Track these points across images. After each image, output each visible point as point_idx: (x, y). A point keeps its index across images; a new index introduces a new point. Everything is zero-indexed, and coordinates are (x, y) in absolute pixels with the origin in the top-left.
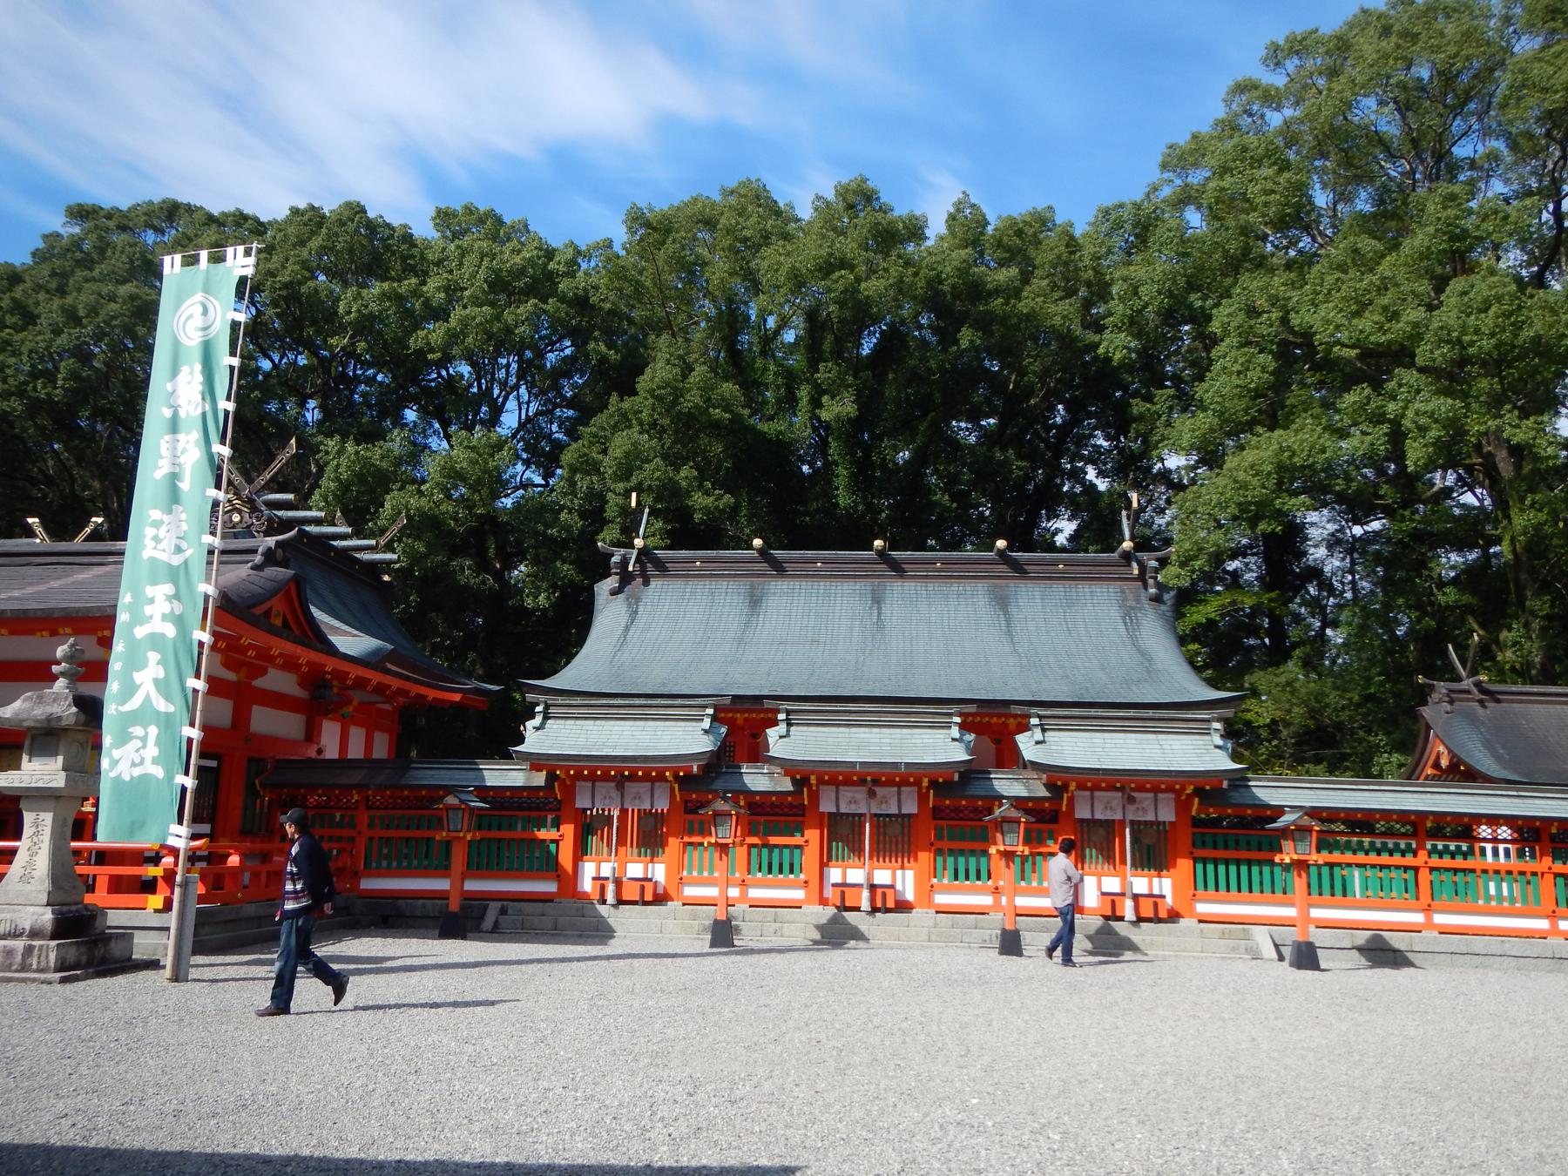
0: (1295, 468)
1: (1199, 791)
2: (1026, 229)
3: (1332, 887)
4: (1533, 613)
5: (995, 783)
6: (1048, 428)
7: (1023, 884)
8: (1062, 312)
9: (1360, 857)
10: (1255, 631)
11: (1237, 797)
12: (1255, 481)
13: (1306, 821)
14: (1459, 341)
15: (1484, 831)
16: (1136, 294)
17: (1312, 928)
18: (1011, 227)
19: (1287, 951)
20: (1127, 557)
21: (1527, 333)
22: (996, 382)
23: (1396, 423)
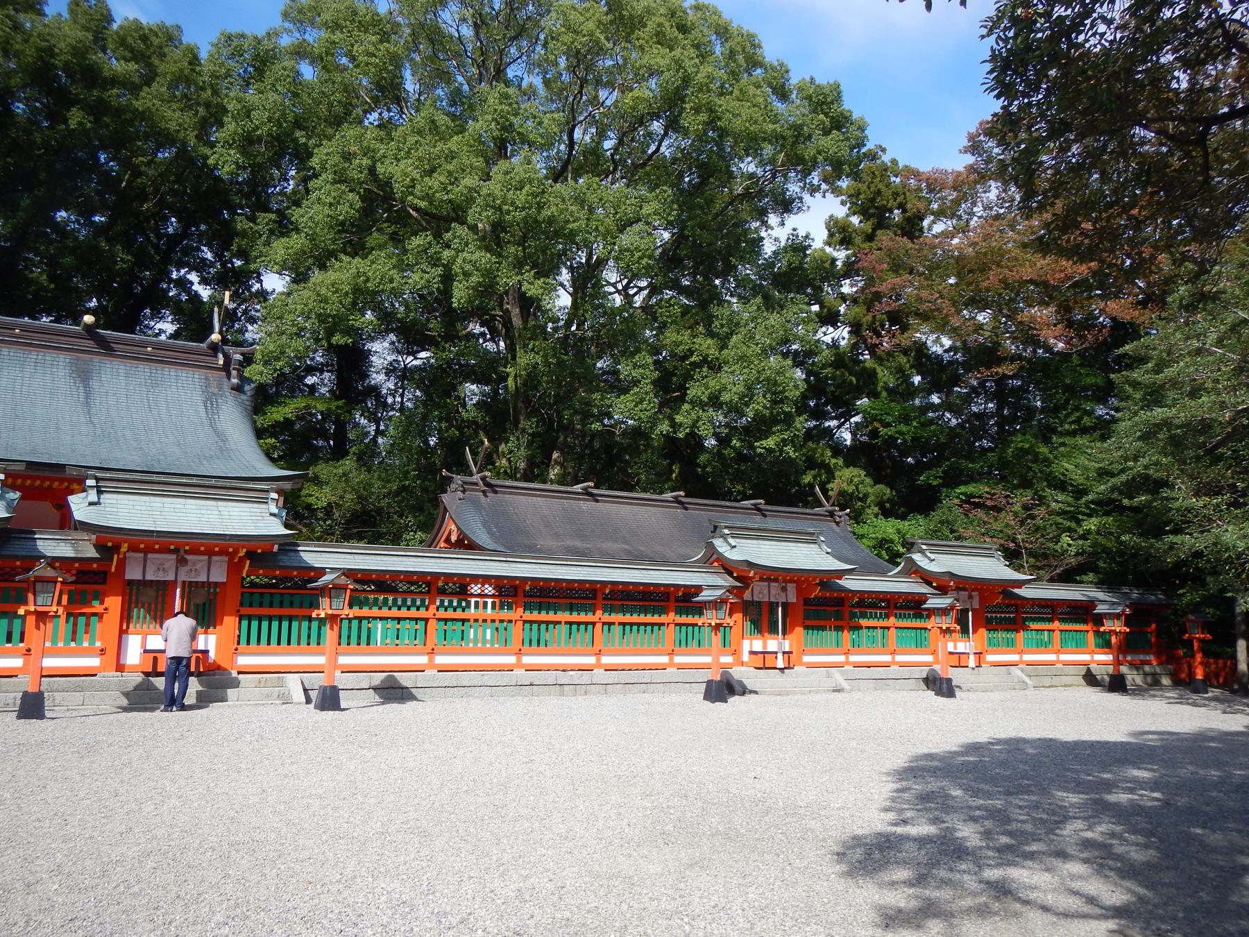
0: (368, 292)
1: (250, 555)
2: (153, 39)
3: (359, 637)
4: (524, 430)
5: (39, 543)
6: (159, 236)
7: (73, 644)
8: (174, 118)
9: (385, 612)
10: (323, 433)
11: (286, 560)
12: (335, 298)
13: (343, 580)
14: (500, 209)
15: (475, 589)
16: (248, 116)
17: (338, 673)
18: (136, 30)
19: (314, 695)
20: (214, 348)
21: (546, 213)
22: (108, 182)
23: (448, 267)
